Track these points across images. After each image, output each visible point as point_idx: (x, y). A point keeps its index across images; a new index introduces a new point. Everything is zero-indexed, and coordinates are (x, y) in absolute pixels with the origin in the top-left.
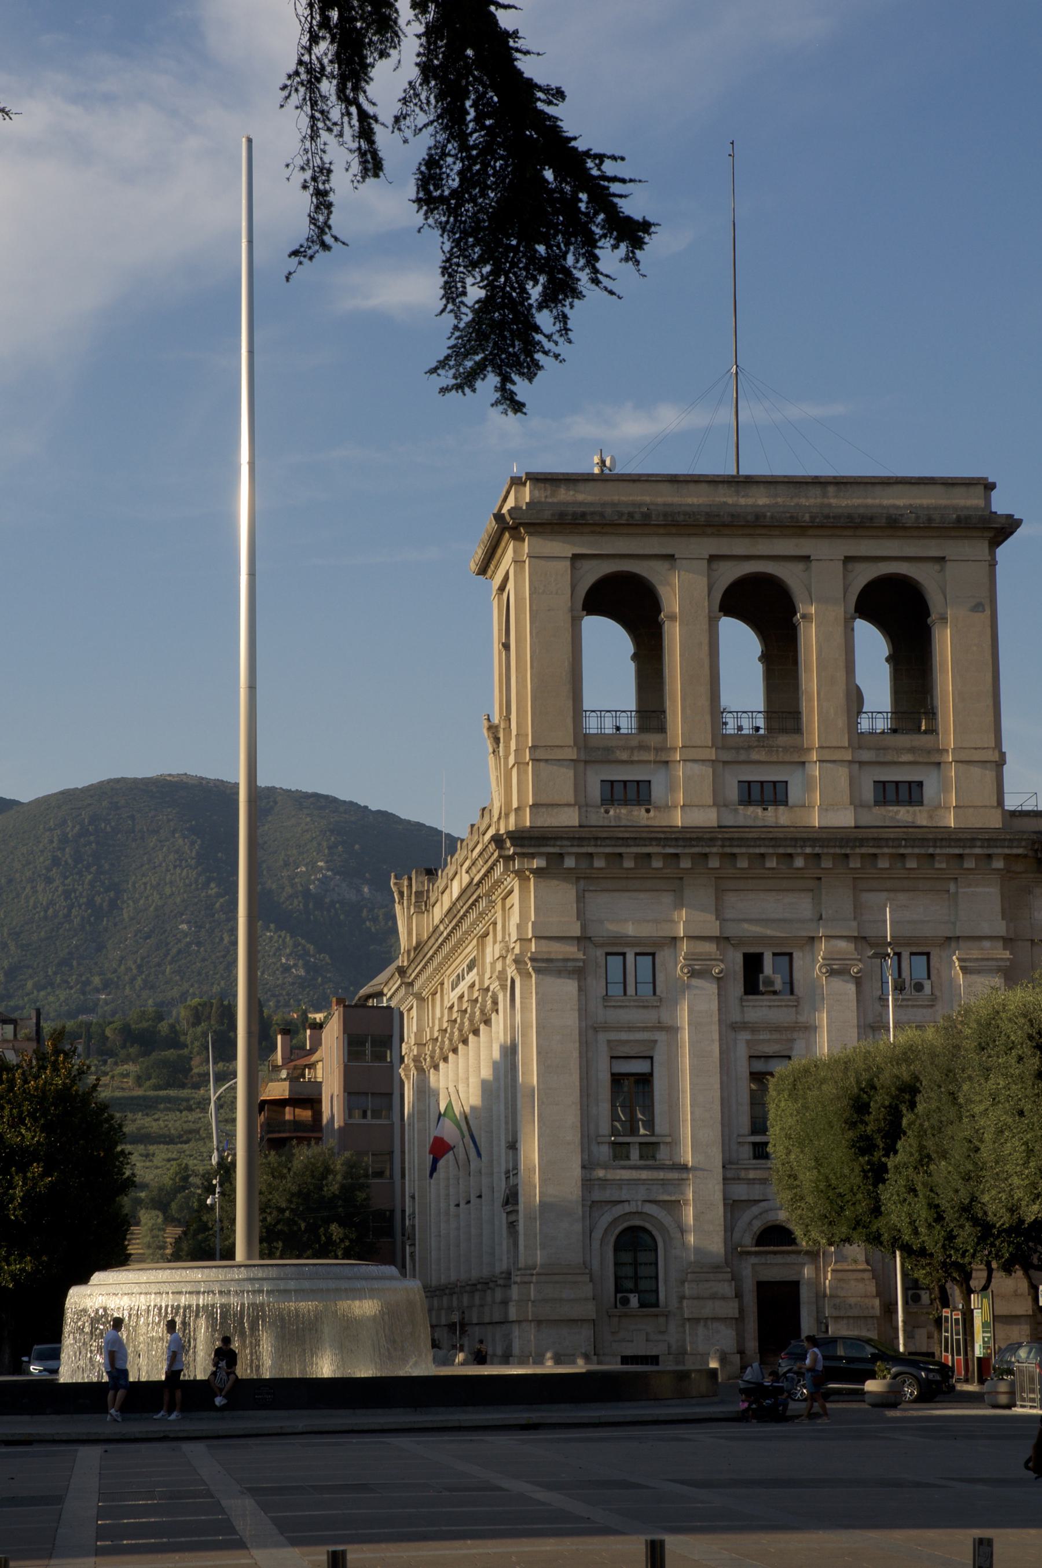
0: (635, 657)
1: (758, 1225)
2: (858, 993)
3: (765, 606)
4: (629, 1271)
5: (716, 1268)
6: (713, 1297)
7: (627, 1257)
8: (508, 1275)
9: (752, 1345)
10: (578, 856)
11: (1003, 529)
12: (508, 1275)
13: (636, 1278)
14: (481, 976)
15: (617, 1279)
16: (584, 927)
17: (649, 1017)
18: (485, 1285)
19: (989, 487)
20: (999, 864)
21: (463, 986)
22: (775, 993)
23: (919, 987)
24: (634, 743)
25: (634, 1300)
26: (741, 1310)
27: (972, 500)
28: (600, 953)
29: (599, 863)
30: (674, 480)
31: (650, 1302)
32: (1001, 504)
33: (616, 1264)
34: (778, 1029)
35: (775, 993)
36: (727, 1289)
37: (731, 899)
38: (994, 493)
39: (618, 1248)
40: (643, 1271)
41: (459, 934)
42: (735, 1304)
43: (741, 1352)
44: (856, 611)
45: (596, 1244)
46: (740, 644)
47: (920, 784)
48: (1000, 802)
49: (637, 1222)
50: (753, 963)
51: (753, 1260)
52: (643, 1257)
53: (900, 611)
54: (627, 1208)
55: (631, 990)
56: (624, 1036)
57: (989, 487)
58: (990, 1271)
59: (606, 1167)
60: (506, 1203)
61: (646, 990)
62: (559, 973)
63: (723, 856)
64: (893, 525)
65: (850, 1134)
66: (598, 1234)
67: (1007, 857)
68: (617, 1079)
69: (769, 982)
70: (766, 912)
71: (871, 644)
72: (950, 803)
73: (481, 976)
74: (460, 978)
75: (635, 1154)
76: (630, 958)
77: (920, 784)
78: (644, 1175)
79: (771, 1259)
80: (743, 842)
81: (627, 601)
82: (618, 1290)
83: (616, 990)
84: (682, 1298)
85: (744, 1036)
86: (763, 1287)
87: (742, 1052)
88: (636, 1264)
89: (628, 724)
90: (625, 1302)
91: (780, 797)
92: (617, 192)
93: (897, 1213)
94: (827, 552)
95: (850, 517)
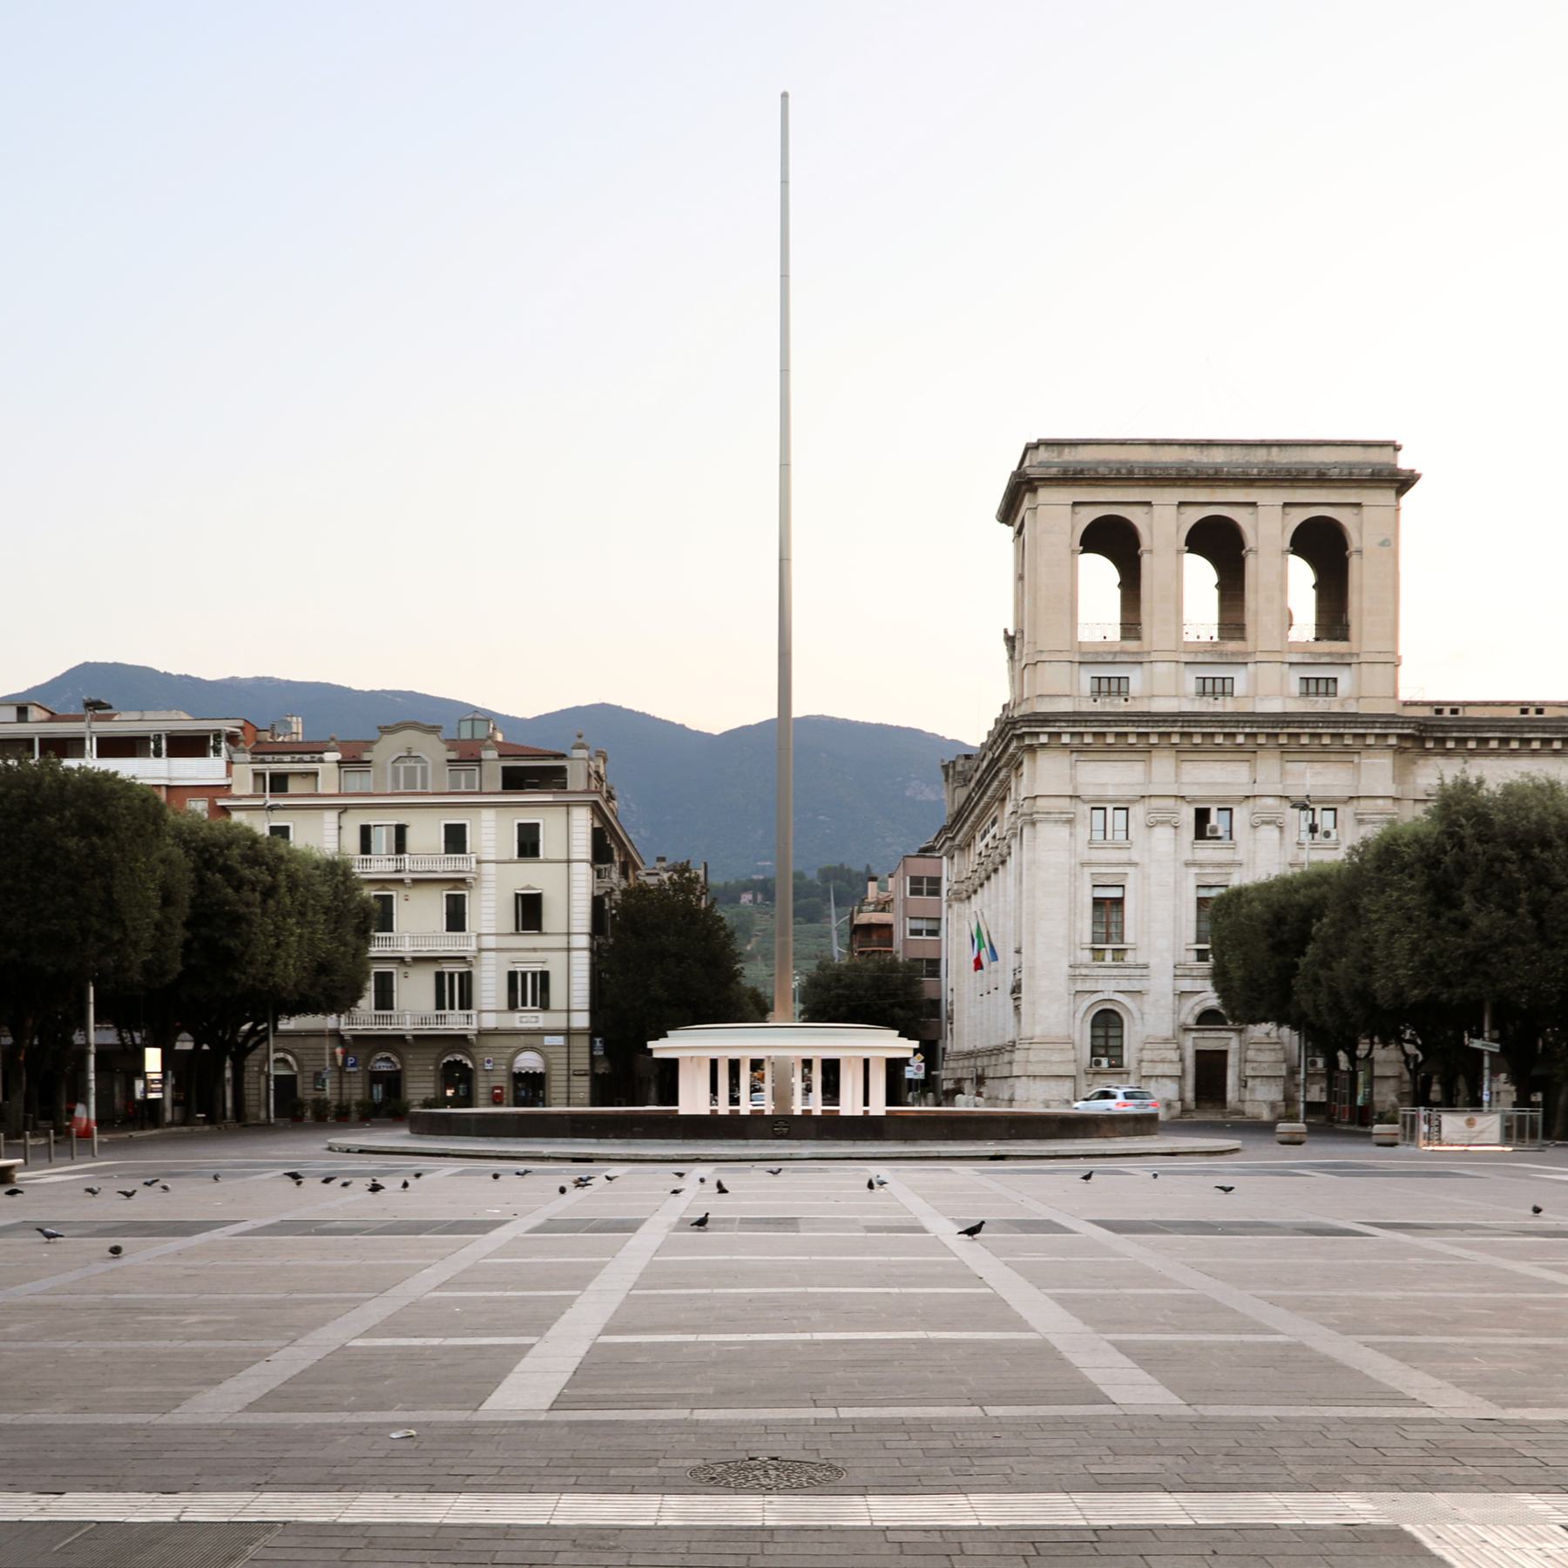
0: (1121, 585)
1: (1198, 1010)
2: (1021, 550)
3: (1219, 542)
4: (1101, 1042)
5: (1166, 1041)
6: (1163, 1061)
7: (1100, 1032)
8: (1014, 1043)
9: (1190, 1095)
10: (1072, 734)
11: (1404, 483)
12: (1014, 1043)
13: (1107, 1047)
14: (1001, 828)
15: (1093, 1047)
16: (1075, 788)
17: (1122, 856)
18: (997, 1051)
19: (1397, 448)
20: (1393, 741)
21: (988, 837)
22: (1218, 838)
23: (1327, 834)
24: (1117, 648)
25: (1105, 1062)
26: (1183, 1071)
27: (1375, 456)
28: (1087, 807)
29: (1088, 739)
30: (1152, 443)
31: (1117, 1063)
32: (1404, 462)
33: (1093, 1037)
34: (1219, 865)
35: (1218, 838)
36: (1174, 1056)
37: (1187, 766)
38: (1400, 453)
39: (1094, 1026)
40: (1112, 1042)
41: (985, 799)
42: (1179, 1066)
43: (1182, 1100)
44: (1293, 543)
45: (1078, 1021)
46: (1200, 574)
47: (1335, 680)
48: (1395, 696)
49: (1108, 1006)
50: (1202, 816)
51: (1194, 1034)
52: (1112, 1032)
53: (1323, 546)
54: (1101, 996)
55: (1109, 836)
56: (1103, 870)
57: (1397, 448)
58: (1372, 1044)
59: (1087, 967)
60: (1013, 992)
61: (1121, 835)
62: (724, 1221)
63: (1182, 734)
64: (1321, 479)
65: (1270, 940)
66: (1079, 1015)
67: (1400, 736)
68: (1098, 903)
69: (1214, 830)
70: (1213, 777)
71: (1301, 576)
72: (1353, 692)
73: (1001, 828)
74: (986, 833)
75: (1109, 956)
76: (1110, 811)
77: (1335, 680)
78: (1115, 972)
79: (1208, 1034)
80: (1198, 723)
81: (1114, 540)
82: (1093, 1055)
83: (1098, 836)
84: (1141, 1061)
85: (1088, 871)
86: (1199, 1053)
87: (1192, 883)
88: (1107, 1037)
89: (1115, 634)
90: (1098, 1063)
91: (1228, 689)
92: (574, 823)
93: (1304, 1000)
94: (1270, 498)
95: (1289, 471)
